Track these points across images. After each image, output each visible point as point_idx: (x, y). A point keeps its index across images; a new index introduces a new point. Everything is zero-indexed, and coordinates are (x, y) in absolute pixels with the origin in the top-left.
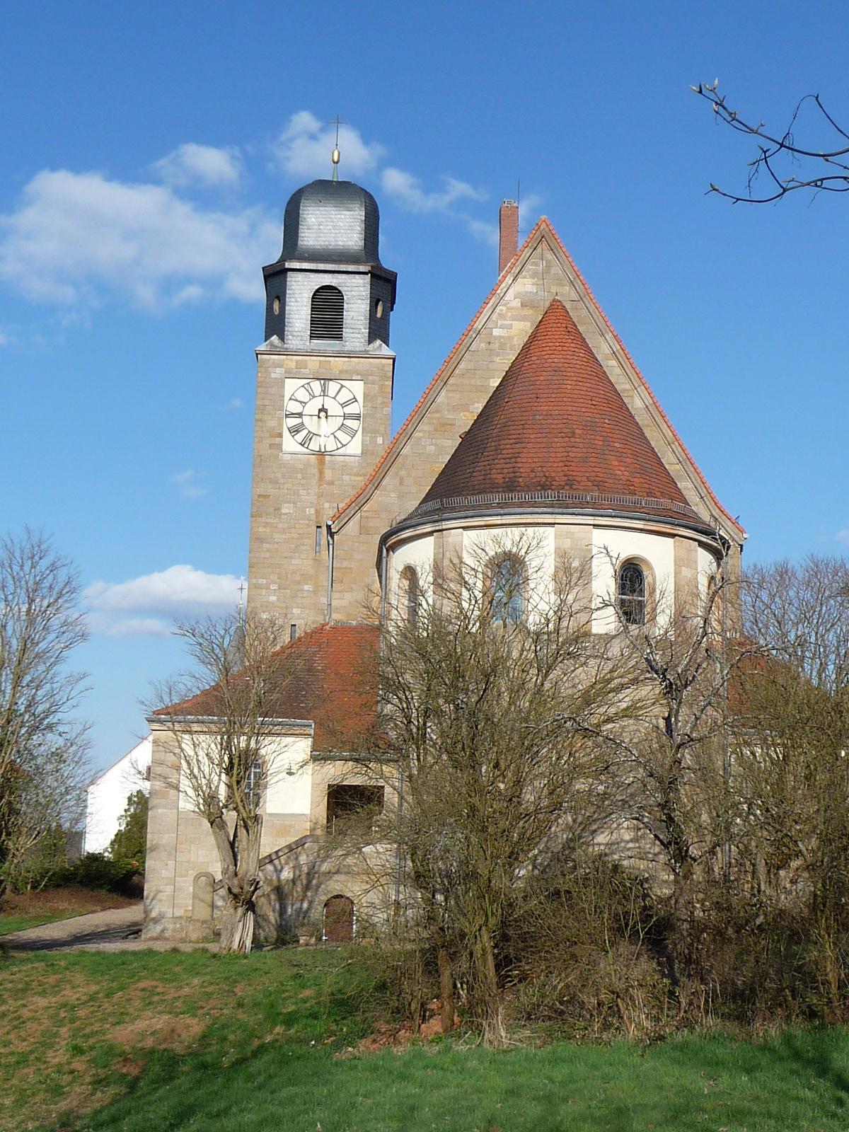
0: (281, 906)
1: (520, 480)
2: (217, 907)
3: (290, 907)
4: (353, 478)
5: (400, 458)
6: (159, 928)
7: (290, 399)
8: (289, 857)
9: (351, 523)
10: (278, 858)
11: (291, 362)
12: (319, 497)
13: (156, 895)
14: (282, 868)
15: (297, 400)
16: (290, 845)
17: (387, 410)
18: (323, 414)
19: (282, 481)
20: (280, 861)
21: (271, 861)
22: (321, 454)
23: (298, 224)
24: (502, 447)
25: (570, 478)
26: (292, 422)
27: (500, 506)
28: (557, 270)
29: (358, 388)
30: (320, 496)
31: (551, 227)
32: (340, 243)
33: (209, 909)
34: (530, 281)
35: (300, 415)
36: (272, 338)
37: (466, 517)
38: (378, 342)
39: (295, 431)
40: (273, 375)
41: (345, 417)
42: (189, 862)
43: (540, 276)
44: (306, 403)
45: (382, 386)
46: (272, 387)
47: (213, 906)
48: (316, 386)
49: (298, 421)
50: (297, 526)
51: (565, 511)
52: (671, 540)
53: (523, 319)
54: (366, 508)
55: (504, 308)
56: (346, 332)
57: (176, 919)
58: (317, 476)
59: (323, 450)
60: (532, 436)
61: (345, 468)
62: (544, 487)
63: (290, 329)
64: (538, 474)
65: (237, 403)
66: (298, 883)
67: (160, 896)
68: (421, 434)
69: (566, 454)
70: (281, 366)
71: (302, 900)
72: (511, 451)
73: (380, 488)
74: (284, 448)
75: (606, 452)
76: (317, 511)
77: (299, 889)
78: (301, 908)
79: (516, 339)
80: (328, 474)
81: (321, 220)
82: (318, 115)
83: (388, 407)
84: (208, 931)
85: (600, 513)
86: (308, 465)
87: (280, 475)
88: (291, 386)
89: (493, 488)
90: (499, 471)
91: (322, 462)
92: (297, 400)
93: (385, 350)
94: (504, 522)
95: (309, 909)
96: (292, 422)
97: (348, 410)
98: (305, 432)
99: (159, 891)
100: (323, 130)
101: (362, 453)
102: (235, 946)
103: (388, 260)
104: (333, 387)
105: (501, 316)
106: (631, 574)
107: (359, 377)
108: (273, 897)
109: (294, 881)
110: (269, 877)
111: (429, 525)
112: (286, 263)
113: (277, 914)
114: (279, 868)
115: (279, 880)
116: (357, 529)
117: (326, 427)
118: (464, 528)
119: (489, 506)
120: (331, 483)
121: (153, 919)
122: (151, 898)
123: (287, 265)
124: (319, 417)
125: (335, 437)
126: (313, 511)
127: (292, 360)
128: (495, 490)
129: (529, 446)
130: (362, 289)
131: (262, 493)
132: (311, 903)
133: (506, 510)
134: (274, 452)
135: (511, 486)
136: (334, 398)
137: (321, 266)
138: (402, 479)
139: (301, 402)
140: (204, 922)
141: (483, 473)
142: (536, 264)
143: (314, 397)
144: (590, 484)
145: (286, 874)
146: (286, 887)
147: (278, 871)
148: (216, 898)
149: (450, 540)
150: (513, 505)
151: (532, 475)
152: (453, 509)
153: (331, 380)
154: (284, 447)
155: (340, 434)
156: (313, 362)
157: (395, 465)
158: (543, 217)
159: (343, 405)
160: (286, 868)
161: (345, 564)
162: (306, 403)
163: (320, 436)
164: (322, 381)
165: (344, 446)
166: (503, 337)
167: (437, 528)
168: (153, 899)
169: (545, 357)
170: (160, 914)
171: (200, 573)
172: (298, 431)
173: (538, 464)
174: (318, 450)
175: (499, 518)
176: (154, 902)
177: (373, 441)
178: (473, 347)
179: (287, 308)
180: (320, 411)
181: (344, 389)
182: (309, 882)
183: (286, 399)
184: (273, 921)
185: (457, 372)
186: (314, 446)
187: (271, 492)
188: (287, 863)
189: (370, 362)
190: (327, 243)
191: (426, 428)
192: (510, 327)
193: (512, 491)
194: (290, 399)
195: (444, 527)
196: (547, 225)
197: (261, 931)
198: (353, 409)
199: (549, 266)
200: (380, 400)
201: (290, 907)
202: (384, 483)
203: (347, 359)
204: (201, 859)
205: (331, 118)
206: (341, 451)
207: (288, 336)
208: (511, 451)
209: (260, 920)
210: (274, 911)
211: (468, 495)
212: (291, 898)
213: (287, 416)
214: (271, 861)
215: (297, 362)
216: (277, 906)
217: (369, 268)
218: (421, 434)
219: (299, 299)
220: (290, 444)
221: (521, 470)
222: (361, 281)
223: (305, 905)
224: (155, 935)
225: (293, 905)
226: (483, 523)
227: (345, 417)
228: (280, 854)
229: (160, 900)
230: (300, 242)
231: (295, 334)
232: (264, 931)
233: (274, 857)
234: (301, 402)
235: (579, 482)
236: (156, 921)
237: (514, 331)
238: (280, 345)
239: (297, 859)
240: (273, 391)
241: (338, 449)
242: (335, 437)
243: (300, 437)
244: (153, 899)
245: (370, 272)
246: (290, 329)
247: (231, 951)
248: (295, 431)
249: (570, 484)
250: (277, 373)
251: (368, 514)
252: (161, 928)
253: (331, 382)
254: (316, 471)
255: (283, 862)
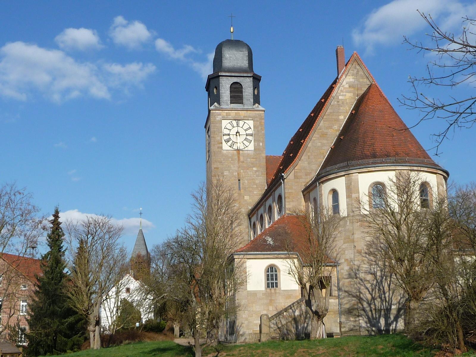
0: (296, 326)
1: (377, 153)
2: (271, 327)
3: (300, 326)
4: (252, 160)
5: (308, 148)
6: (243, 338)
7: (225, 128)
8: (298, 306)
9: (291, 174)
10: (294, 306)
11: (224, 113)
12: (238, 168)
13: (241, 325)
14: (295, 311)
15: (227, 129)
16: (297, 301)
17: (263, 132)
18: (238, 134)
19: (223, 162)
20: (294, 308)
21: (291, 308)
22: (238, 150)
23: (222, 57)
24: (366, 141)
25: (397, 152)
26: (226, 138)
27: (372, 163)
28: (361, 73)
29: (251, 123)
30: (239, 167)
31: (358, 56)
32: (239, 65)
33: (269, 328)
34: (352, 77)
35: (229, 135)
36: (215, 104)
37: (360, 168)
38: (257, 105)
39: (227, 141)
40: (217, 119)
41: (247, 135)
42: (253, 311)
43: (355, 75)
44: (231, 130)
45: (260, 122)
46: (217, 124)
47: (270, 327)
48: (234, 123)
49: (228, 137)
50: (231, 180)
51: (400, 164)
52: (435, 175)
53: (350, 92)
54: (296, 168)
55: (342, 88)
56: (245, 101)
57: (250, 334)
58: (237, 159)
59: (239, 149)
60: (378, 136)
61: (248, 156)
62: (388, 156)
63: (222, 100)
64: (384, 151)
65: (94, 139)
66: (302, 316)
67: (243, 325)
68: (315, 138)
69: (392, 143)
70: (220, 115)
71: (304, 323)
72: (370, 142)
73: (301, 160)
74: (223, 148)
75: (406, 142)
76: (238, 174)
77: (303, 319)
78: (304, 326)
79: (348, 100)
80: (242, 159)
81: (230, 56)
82: (126, 18)
83: (263, 130)
84: (269, 337)
85: (413, 165)
86: (233, 155)
87: (222, 160)
88: (225, 123)
89: (367, 157)
90: (367, 150)
91: (239, 154)
92: (227, 129)
93: (261, 108)
94: (376, 170)
95: (307, 326)
96: (226, 138)
97: (248, 132)
98: (231, 141)
99: (242, 323)
100: (128, 24)
101: (254, 149)
102: (318, 336)
103: (257, 71)
104: (241, 123)
105: (342, 91)
106: (424, 187)
107: (251, 119)
108: (293, 322)
109: (300, 316)
110: (290, 315)
111: (343, 172)
112: (219, 73)
113: (295, 329)
114: (294, 310)
115: (294, 315)
116: (293, 176)
117: (240, 139)
118: (359, 173)
119: (368, 164)
120: (243, 162)
121: (241, 335)
122: (239, 326)
123: (220, 74)
124: (236, 135)
125: (243, 143)
126: (236, 174)
127: (224, 112)
128: (368, 157)
129: (377, 140)
130: (249, 83)
131: (216, 167)
132: (308, 324)
133: (377, 165)
134: (220, 150)
135: (374, 156)
136: (242, 127)
137: (233, 74)
138: (309, 156)
139: (229, 129)
140: (267, 334)
141: (360, 151)
142: (353, 70)
143: (234, 127)
144: (404, 154)
145: (297, 313)
146: (298, 318)
147: (294, 312)
148: (271, 324)
149: (353, 178)
150: (378, 163)
151: (382, 151)
152: (353, 166)
153: (240, 120)
154: (223, 148)
155: (245, 142)
156: (233, 113)
157: (306, 151)
158: (355, 52)
159: (246, 130)
160: (297, 311)
161: (290, 191)
162: (231, 130)
163: (237, 143)
164: (237, 121)
165: (247, 147)
166: (343, 99)
167: (347, 173)
168: (240, 327)
169: (375, 106)
170: (243, 333)
171: (80, 213)
172: (228, 141)
173: (383, 147)
174: (237, 148)
175: (374, 168)
176: (241, 328)
177: (259, 145)
178: (332, 104)
179: (220, 91)
180: (237, 133)
181: (245, 123)
182: (306, 315)
183: (223, 128)
184: (294, 332)
185: (327, 113)
186: (235, 147)
187: (220, 166)
188: (297, 309)
189: (255, 113)
190: (234, 65)
191: (317, 136)
192: (345, 95)
193: (376, 158)
194: (225, 128)
195: (350, 173)
196: (357, 55)
197: (289, 336)
198: (250, 132)
199: (358, 71)
200: (260, 128)
201: (300, 326)
202: (302, 158)
203: (246, 112)
204: (257, 310)
205: (130, 18)
206: (246, 149)
207: (222, 103)
208: (370, 142)
209: (288, 331)
210: (294, 328)
211: (359, 160)
212: (300, 322)
213: (224, 135)
214: (291, 308)
215: (226, 113)
216: (295, 326)
217: (252, 75)
218: (315, 138)
219: (225, 88)
220: (226, 147)
221: (377, 150)
222: (249, 80)
223: (306, 325)
224: (242, 341)
225: (301, 325)
226: (367, 171)
227: (247, 135)
228: (294, 305)
229: (243, 327)
230: (223, 65)
231: (224, 102)
232: (291, 336)
233: (292, 306)
234: (229, 129)
235: (400, 154)
236: (242, 335)
237: (347, 97)
238: (218, 106)
239: (301, 307)
240: (218, 125)
241: (245, 148)
242: (243, 143)
243: (229, 143)
244: (240, 327)
245: (252, 76)
246: (222, 100)
247: (316, 339)
248: (227, 141)
249: (397, 154)
250: (219, 118)
251: (297, 171)
252: (244, 338)
253: (240, 121)
254: (236, 157)
255: (295, 308)
